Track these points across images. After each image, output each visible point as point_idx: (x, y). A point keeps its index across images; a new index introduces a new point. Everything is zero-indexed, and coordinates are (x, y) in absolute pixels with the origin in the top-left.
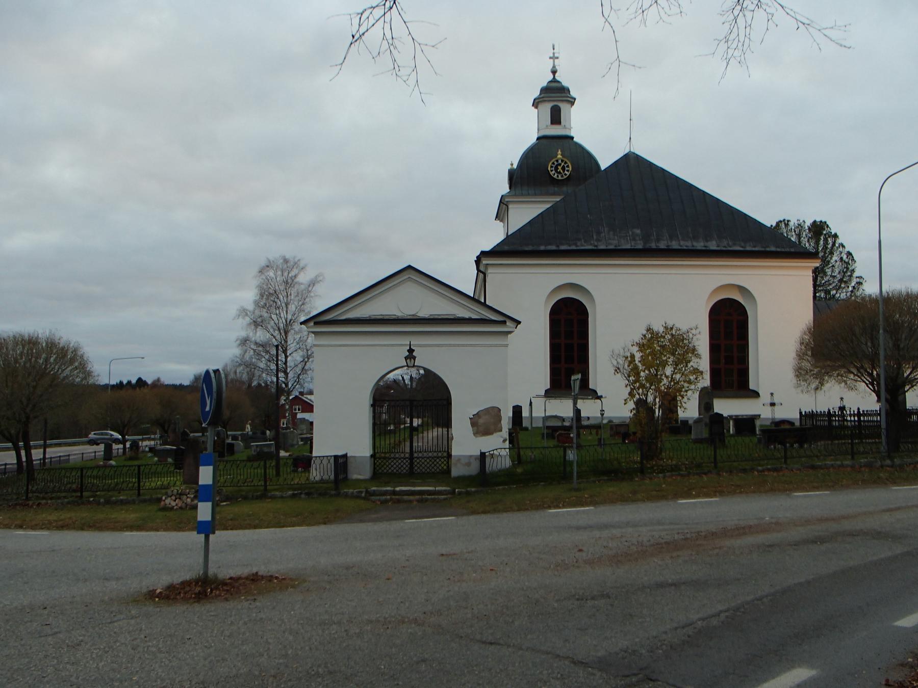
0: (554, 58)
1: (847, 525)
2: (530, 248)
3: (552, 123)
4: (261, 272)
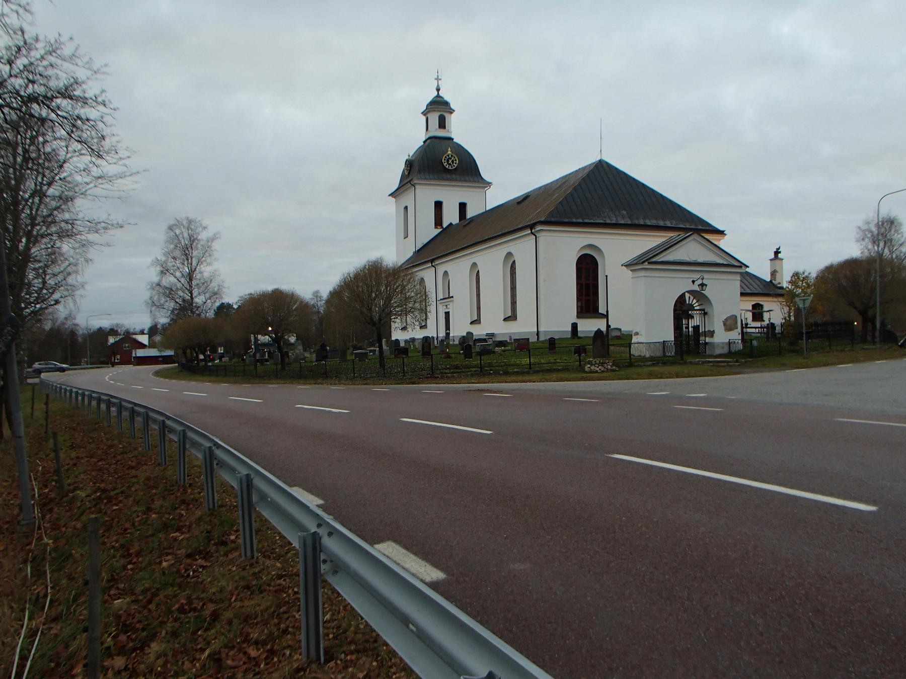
0: (438, 79)
1: (208, 463)
2: (566, 220)
3: (440, 127)
4: (171, 228)
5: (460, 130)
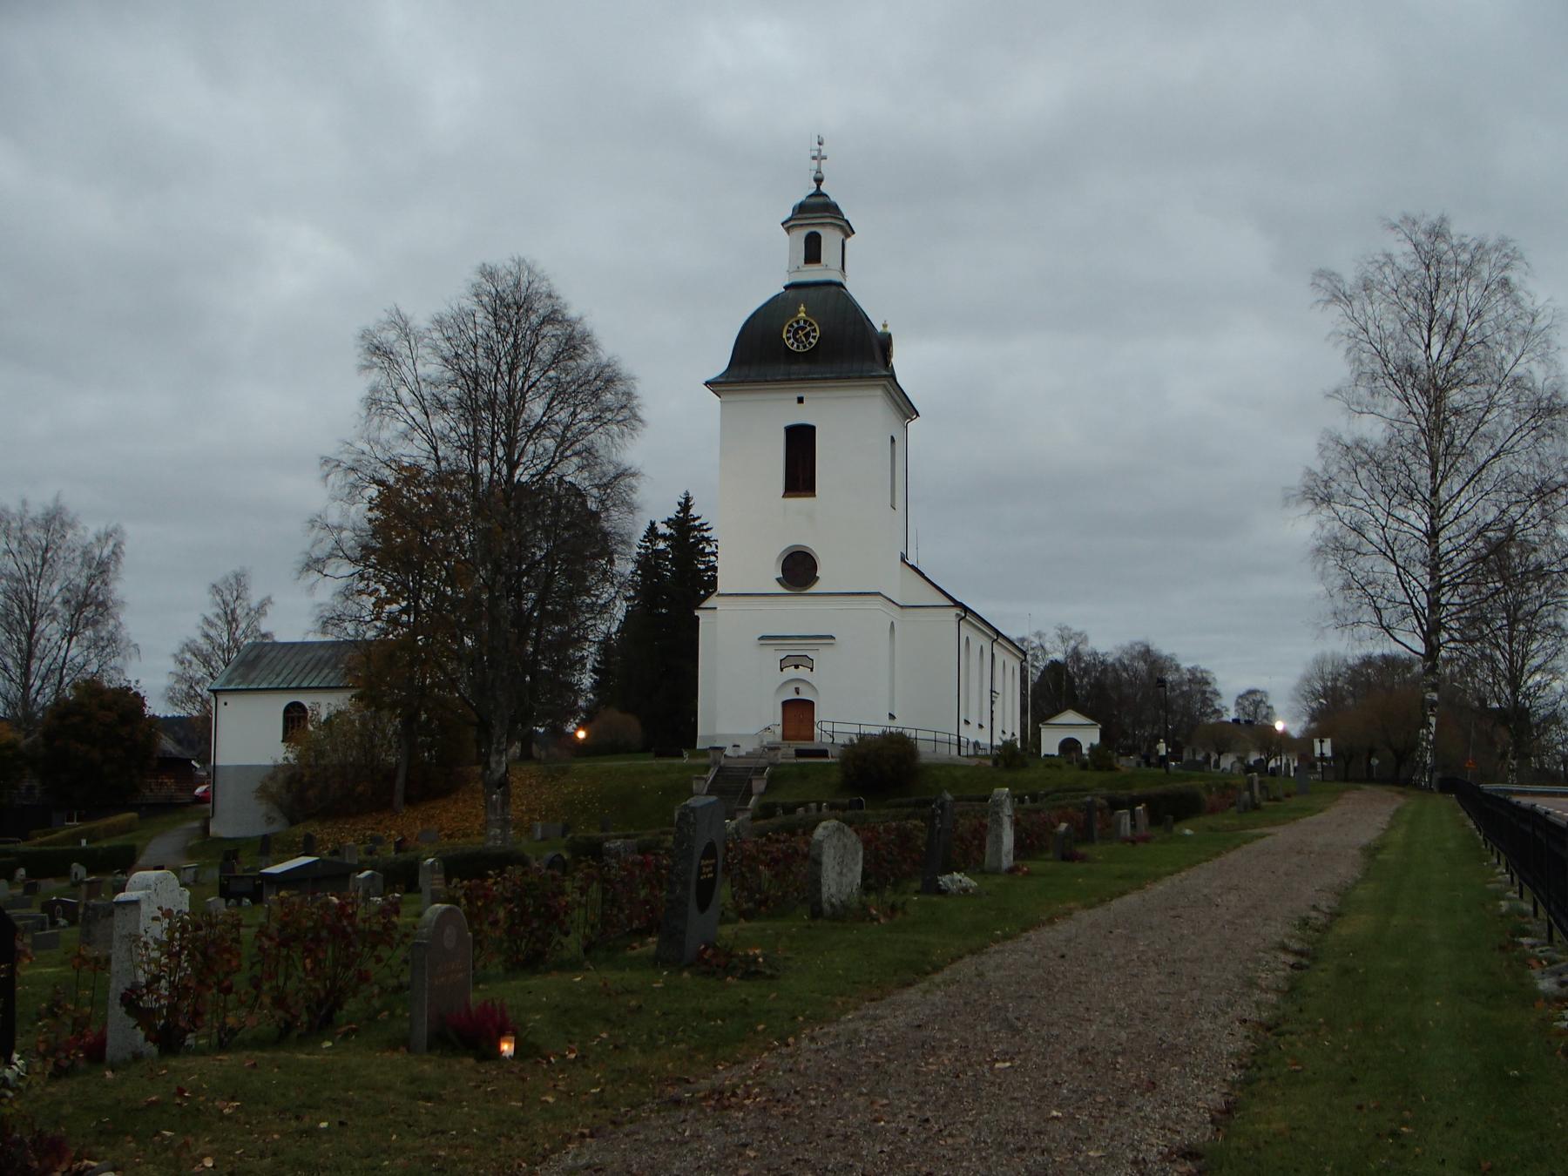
5: (874, 281)
